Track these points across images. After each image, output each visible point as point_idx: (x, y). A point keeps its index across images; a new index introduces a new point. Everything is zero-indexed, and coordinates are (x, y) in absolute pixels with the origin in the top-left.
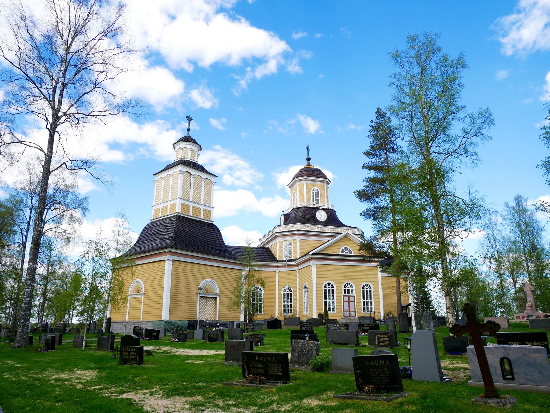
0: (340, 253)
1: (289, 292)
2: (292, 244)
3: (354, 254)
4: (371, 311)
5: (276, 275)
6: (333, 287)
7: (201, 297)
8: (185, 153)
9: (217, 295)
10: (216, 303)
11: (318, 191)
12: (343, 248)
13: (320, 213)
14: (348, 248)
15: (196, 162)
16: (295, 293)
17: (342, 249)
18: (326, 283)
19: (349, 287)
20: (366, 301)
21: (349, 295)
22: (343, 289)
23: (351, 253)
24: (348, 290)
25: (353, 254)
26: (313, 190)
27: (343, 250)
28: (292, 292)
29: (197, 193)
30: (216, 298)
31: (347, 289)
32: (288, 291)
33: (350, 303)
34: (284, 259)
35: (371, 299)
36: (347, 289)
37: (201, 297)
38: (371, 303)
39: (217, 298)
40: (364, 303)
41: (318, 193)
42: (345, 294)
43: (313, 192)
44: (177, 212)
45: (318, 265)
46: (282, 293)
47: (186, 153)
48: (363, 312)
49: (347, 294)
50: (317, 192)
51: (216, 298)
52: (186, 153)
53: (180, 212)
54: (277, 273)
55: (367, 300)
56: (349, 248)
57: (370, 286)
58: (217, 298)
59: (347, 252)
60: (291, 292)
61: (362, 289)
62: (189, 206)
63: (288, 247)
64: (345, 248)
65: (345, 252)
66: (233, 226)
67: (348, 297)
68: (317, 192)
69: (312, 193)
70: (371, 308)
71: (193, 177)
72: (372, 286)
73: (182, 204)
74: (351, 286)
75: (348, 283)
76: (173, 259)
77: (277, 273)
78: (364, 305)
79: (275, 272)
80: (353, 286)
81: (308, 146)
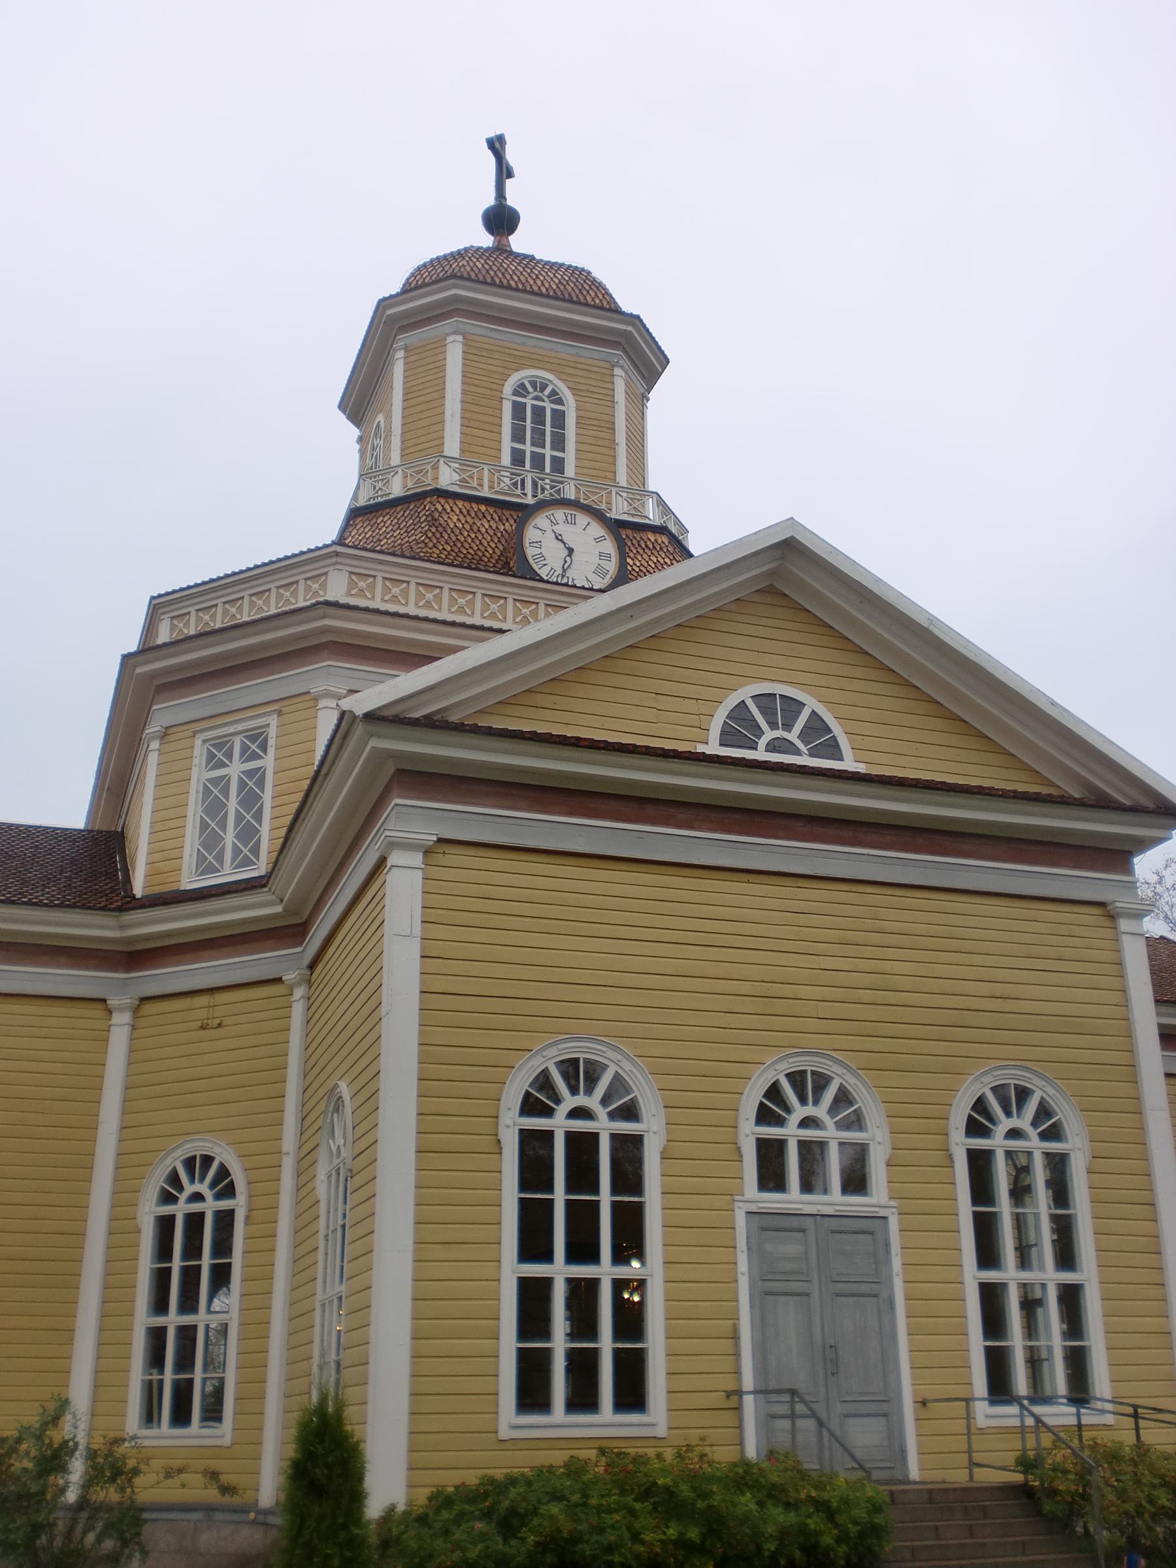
0: (713, 748)
1: (210, 1206)
2: (272, 742)
3: (861, 768)
4: (1080, 1392)
5: (103, 1038)
6: (629, 1112)
11: (560, 401)
12: (746, 693)
13: (562, 529)
14: (793, 706)
16: (263, 1215)
17: (732, 701)
18: (548, 1060)
19: (820, 1111)
20: (1009, 1274)
21: (812, 1203)
22: (749, 1132)
23: (833, 750)
24: (811, 1152)
25: (849, 763)
26: (520, 390)
27: (740, 712)
28: (239, 1204)
31: (791, 1132)
32: (203, 1188)
33: (966, 1432)
34: (189, 881)
35: (1066, 1257)
36: (791, 1132)
38: (1071, 1297)
40: (991, 1296)
41: (559, 419)
42: (773, 1200)
43: (518, 410)
45: (455, 856)
46: (148, 1211)
48: (985, 1413)
49: (793, 1198)
50: (549, 406)
54: (122, 1020)
55: (620, 1257)
56: (811, 704)
57: (1044, 1112)
59: (793, 736)
60: (225, 1204)
61: (960, 1144)
63: (235, 769)
64: (765, 701)
65: (769, 735)
67: (963, 1403)
68: (549, 406)
69: (507, 409)
70: (1077, 1361)
72: (1067, 1114)
74: (843, 1098)
75: (808, 1064)
77: (122, 1020)
78: (994, 1323)
79: (95, 1011)
80: (867, 1102)
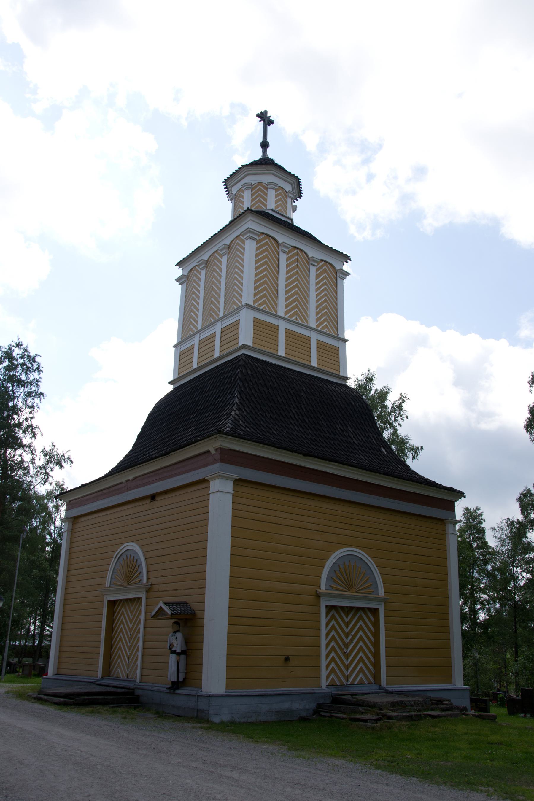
7: (330, 608)
8: (259, 195)
9: (380, 600)
10: (378, 690)
15: (290, 222)
29: (281, 206)
30: (375, 611)
37: (330, 608)
39: (378, 609)
44: (240, 344)
47: (262, 197)
51: (375, 611)
52: (262, 197)
53: (251, 344)
58: (378, 609)
62: (276, 328)
66: (422, 324)
71: (284, 252)
73: (257, 321)
76: (237, 477)
81: (531, 391)
